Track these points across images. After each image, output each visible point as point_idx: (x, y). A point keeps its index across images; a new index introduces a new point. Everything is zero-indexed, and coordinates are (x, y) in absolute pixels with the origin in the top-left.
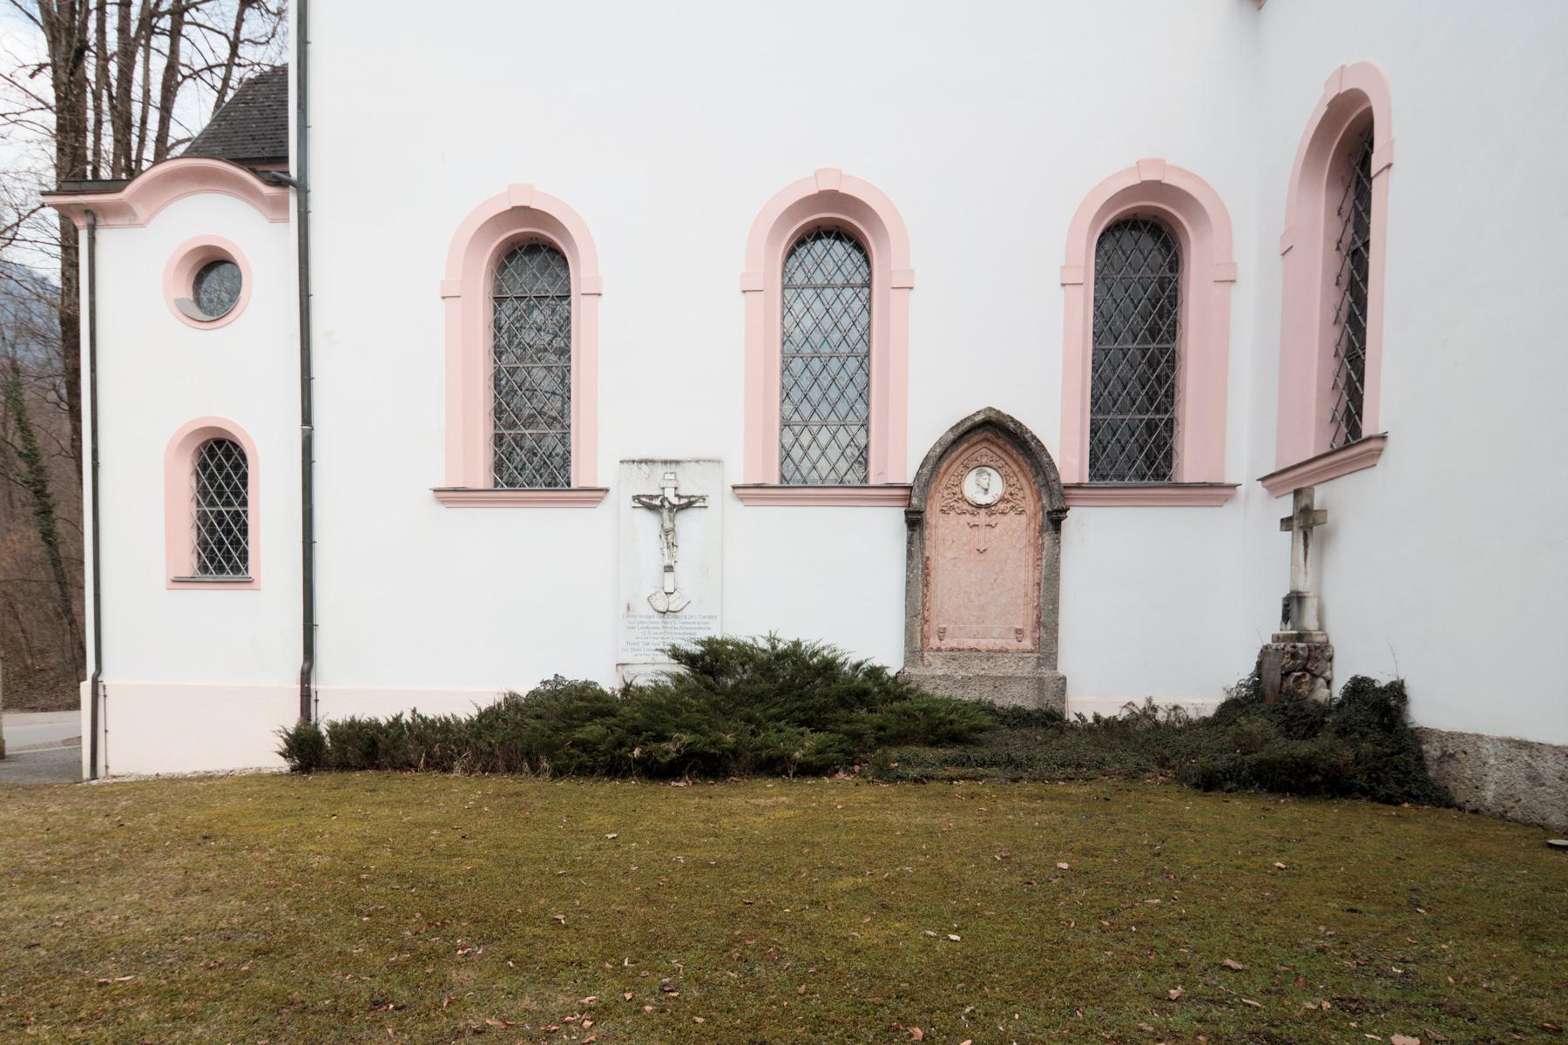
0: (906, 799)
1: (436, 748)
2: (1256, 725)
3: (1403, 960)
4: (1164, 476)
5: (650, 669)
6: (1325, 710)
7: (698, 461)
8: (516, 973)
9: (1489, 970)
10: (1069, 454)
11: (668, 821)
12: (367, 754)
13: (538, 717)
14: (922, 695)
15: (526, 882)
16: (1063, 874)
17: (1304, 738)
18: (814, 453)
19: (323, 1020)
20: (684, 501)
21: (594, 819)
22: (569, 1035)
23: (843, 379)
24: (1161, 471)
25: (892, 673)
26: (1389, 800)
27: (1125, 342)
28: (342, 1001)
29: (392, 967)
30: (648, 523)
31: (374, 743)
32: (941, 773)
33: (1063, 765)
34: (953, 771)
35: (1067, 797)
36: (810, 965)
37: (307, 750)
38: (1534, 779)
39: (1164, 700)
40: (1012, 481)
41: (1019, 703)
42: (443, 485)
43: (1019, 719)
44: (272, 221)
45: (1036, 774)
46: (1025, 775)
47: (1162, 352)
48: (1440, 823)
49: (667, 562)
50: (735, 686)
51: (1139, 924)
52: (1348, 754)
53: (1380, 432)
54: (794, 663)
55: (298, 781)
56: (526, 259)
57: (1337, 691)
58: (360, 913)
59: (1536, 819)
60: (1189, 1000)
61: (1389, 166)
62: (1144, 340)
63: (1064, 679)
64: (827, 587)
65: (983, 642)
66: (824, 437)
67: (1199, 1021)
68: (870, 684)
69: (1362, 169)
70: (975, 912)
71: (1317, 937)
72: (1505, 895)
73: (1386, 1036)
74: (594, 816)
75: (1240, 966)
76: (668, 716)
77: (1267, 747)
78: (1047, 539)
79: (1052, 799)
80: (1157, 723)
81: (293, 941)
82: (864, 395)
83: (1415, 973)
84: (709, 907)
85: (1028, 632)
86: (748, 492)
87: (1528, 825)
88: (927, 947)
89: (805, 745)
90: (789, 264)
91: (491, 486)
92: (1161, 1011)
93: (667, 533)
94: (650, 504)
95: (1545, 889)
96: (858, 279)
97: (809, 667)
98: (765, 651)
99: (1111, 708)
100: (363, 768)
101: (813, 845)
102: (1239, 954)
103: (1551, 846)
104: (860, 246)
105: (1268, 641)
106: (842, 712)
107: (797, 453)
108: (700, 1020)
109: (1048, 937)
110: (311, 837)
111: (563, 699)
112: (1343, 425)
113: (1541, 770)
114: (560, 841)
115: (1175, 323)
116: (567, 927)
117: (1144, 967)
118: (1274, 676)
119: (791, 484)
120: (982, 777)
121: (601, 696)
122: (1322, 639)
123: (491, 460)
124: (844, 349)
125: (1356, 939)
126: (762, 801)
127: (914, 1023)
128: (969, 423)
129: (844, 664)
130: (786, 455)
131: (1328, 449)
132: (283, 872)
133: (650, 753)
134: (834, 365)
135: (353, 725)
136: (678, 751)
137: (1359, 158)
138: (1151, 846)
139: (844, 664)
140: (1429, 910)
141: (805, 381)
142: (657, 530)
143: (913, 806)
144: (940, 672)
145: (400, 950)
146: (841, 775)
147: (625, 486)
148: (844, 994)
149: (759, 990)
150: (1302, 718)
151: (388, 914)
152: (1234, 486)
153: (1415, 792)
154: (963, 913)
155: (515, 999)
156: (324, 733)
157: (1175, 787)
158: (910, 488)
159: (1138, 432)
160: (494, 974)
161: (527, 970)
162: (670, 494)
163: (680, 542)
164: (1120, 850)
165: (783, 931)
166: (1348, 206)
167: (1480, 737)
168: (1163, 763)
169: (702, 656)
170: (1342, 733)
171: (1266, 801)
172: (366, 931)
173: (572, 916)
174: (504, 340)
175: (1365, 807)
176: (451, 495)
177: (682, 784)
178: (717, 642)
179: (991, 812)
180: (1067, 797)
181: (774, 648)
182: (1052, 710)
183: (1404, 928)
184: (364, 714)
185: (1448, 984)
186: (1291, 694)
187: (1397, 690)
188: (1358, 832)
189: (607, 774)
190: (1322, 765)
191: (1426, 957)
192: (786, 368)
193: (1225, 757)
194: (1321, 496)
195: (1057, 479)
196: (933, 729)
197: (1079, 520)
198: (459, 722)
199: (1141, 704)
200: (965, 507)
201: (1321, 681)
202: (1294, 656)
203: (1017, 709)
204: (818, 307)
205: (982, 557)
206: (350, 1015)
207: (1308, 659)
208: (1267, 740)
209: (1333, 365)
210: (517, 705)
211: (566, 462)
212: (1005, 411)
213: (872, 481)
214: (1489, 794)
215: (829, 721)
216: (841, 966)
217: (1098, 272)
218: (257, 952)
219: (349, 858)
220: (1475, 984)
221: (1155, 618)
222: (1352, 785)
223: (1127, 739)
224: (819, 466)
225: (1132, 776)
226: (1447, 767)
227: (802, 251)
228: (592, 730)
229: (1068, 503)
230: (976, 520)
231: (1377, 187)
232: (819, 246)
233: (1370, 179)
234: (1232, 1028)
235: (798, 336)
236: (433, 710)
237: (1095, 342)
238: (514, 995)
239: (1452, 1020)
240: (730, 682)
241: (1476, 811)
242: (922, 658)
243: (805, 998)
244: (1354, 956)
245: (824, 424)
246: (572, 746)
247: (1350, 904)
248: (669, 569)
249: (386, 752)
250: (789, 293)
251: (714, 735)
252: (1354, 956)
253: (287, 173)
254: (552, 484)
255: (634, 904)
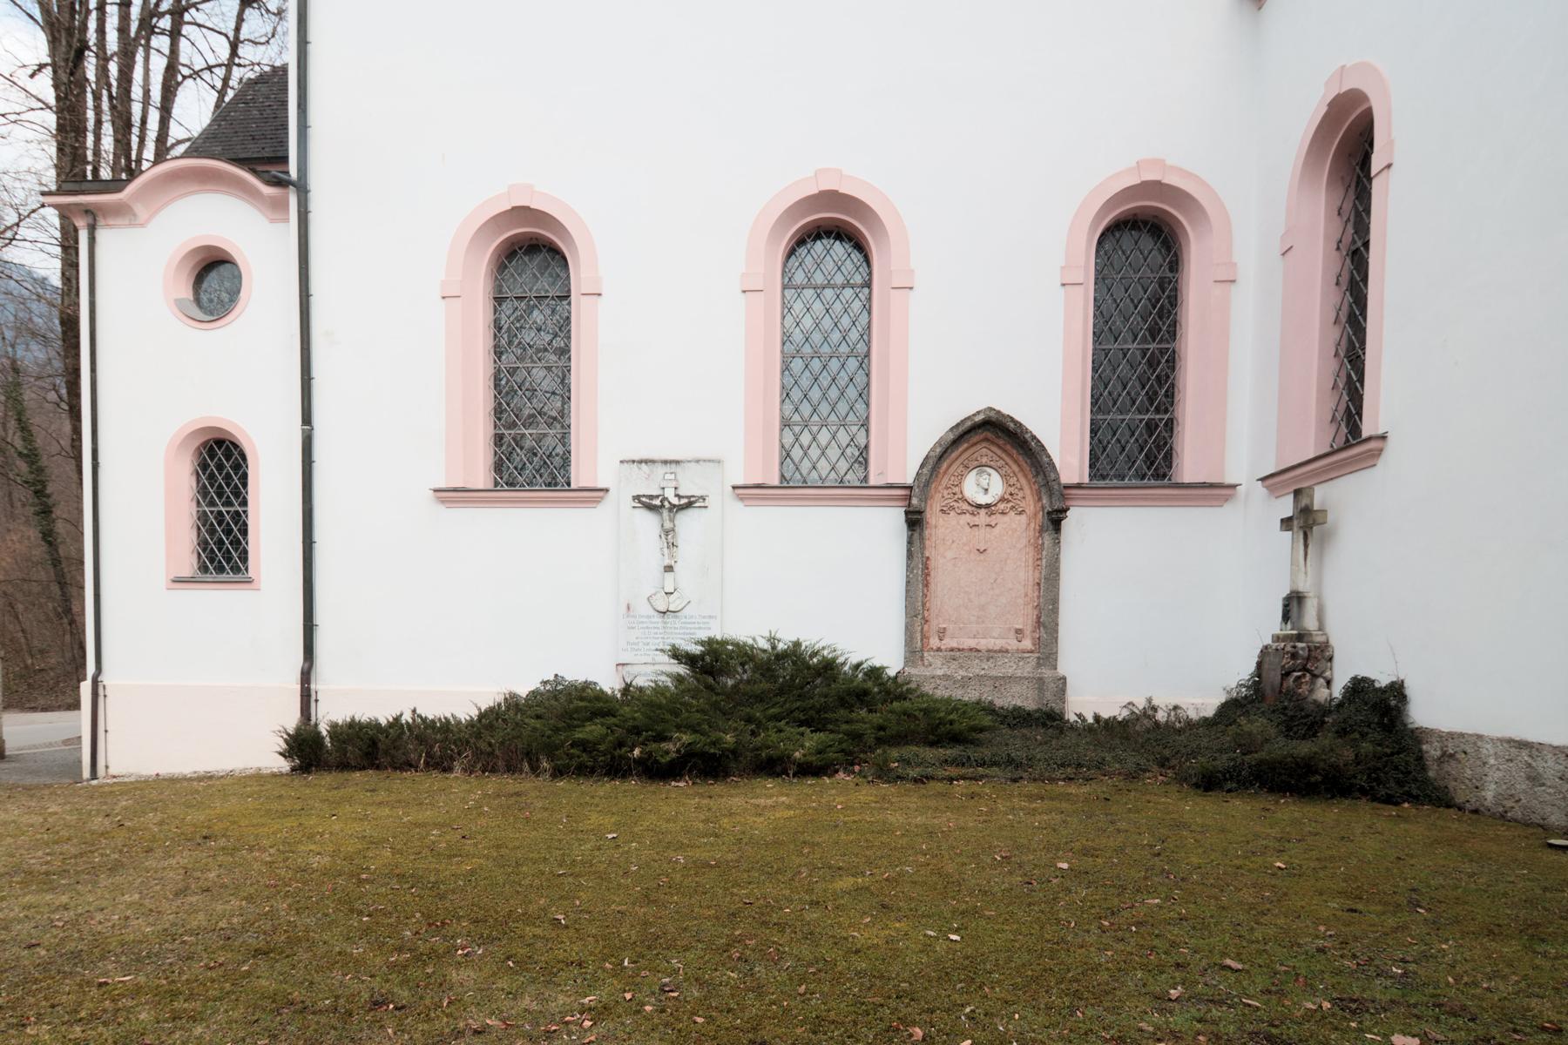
0: (906, 799)
1: (436, 748)
2: (1256, 725)
3: (1403, 960)
4: (1164, 476)
5: (650, 669)
6: (1325, 710)
7: (698, 461)
8: (516, 973)
9: (1489, 970)
10: (1069, 454)
11: (668, 821)
12: (367, 754)
13: (538, 717)
14: (922, 695)
15: (526, 882)
16: (1063, 874)
17: (1304, 738)
18: (814, 453)
19: (323, 1020)
20: (684, 501)
21: (594, 819)
22: (569, 1035)
23: (843, 379)
24: (1161, 471)
25: (892, 673)
26: (1389, 800)
27: (1125, 342)
28: (342, 1001)
29: (392, 967)
30: (648, 523)
31: (374, 743)
32: (941, 773)
33: (1063, 765)
34: (953, 771)
35: (1067, 797)
36: (810, 965)
37: (307, 750)
38: (1534, 779)
39: (1164, 700)
40: (1012, 481)
41: (1019, 703)
42: (443, 485)
43: (1019, 719)
44: (272, 221)
45: (1036, 774)
46: (1025, 775)
47: (1162, 352)
48: (1440, 823)
49: (667, 562)
50: (735, 686)
51: (1139, 924)
52: (1348, 754)
53: (1380, 432)
54: (794, 663)
55: (298, 781)
56: (526, 259)
57: (1337, 691)
58: (360, 913)
59: (1536, 819)
60: (1189, 1000)
61: (1389, 166)
62: (1144, 340)
63: (1064, 679)
64: (827, 587)
65: (983, 642)
66: (824, 437)
67: (1199, 1021)
68: (870, 684)
69: (1362, 169)
70: (975, 912)
71: (1317, 937)
72: (1505, 895)
73: (1386, 1036)
74: (594, 816)
75: (1240, 966)
76: (668, 716)
77: (1267, 747)
78: (1047, 539)
79: (1052, 799)
80: (1157, 723)
81: (293, 941)
82: (864, 395)
83: (1415, 973)
84: (709, 907)
85: (1028, 632)
86: (748, 492)
87: (1528, 825)
88: (927, 947)
89: (805, 745)
90: (789, 264)
91: (491, 486)
92: (1161, 1011)
93: (667, 533)
94: (650, 504)
95: (1545, 889)
96: (858, 279)
97: (809, 667)
98: (765, 651)
99: (1111, 708)
100: (363, 768)
101: (813, 845)
102: (1239, 954)
103: (1551, 846)
104: (860, 246)
105: (1268, 641)
106: (842, 712)
107: (797, 453)
108: (700, 1020)
109: (1048, 937)
110: (311, 837)
111: (563, 699)
112: (1343, 425)
113: (1541, 770)
114: (560, 841)
115: (1175, 323)
116: (567, 927)
117: (1144, 967)
118: (1274, 676)
119: (791, 484)
120: (982, 777)
121: (601, 696)
122: (1322, 639)
123: (491, 460)
124: (844, 349)
125: (1356, 939)
126: (762, 801)
127: (914, 1023)
128: (969, 423)
129: (844, 664)
130: (786, 455)
131: (1328, 449)
132: (283, 872)
133: (650, 753)
134: (834, 365)
135: (353, 725)
136: (678, 751)
137: (1359, 158)
138: (1151, 846)
139: (844, 664)
140: (1429, 910)
141: (805, 381)
142: (657, 530)
143: (913, 806)
144: (940, 672)
145: (400, 950)
146: (841, 775)
147: (625, 486)
148: (844, 994)
149: (759, 990)
150: (1302, 718)
151: (388, 914)
152: (1234, 486)
153: (1415, 792)
154: (963, 913)
155: (515, 999)
156: (324, 733)
157: (1175, 787)
158: (910, 488)
159: (1138, 432)
160: (494, 974)
161: (527, 970)
162: (670, 494)
163: (680, 542)
164: (1120, 850)
165: (783, 931)
166: (1348, 206)
167: (1480, 737)
168: (1163, 763)
169: (702, 656)
170: (1342, 733)
171: (1266, 801)
172: (366, 931)
173: (572, 916)
174: (504, 340)
175: (1365, 807)
176: (451, 495)
177: (682, 784)
178: (717, 642)
179: (991, 812)
180: (1067, 797)
181: (774, 648)
182: (1052, 710)
183: (1404, 928)
184: (364, 714)
185: (1448, 984)
186: (1291, 694)
187: (1397, 690)
188: (1358, 832)
189: (607, 774)
190: (1322, 765)
191: (1426, 957)
192: (786, 368)
193: (1225, 757)
194: (1321, 496)
195: (1057, 479)
196: (933, 729)
197: (1079, 520)
198: (459, 722)
199: (1141, 704)
200: (965, 507)
201: (1321, 681)
202: (1294, 656)
203: (1017, 709)
204: (818, 307)
205: (982, 557)
206: (350, 1015)
207: (1308, 659)
208: (1267, 740)
209: (1333, 365)
210: (517, 705)
211: (566, 462)
212: (1005, 411)
213: (872, 481)
214: (1489, 794)
215: (829, 721)
216: (841, 966)
217: (1098, 272)
218: (257, 952)
219: (349, 858)
220: (1475, 984)
221: (1155, 618)
222: (1352, 785)
223: (1127, 739)
224: (819, 466)
225: (1132, 776)
226: (1447, 767)
227: (802, 251)
228: (592, 730)
229: (1068, 503)
230: (976, 520)
231: (1377, 187)
232: (819, 246)
233: (1370, 179)
234: (1232, 1028)
235: (798, 336)
236: (433, 710)
237: (1095, 342)
238: (514, 995)
239: (1452, 1020)
240: (730, 682)
241: (1476, 811)
242: (922, 658)
243: (805, 998)
244: (1354, 956)
245: (824, 424)
246: (572, 746)
247: (1350, 904)
248: (669, 569)
249: (386, 752)
250: (789, 293)
251: (714, 735)
252: (1354, 956)
253: (287, 173)
254: (552, 484)
255: (634, 904)
